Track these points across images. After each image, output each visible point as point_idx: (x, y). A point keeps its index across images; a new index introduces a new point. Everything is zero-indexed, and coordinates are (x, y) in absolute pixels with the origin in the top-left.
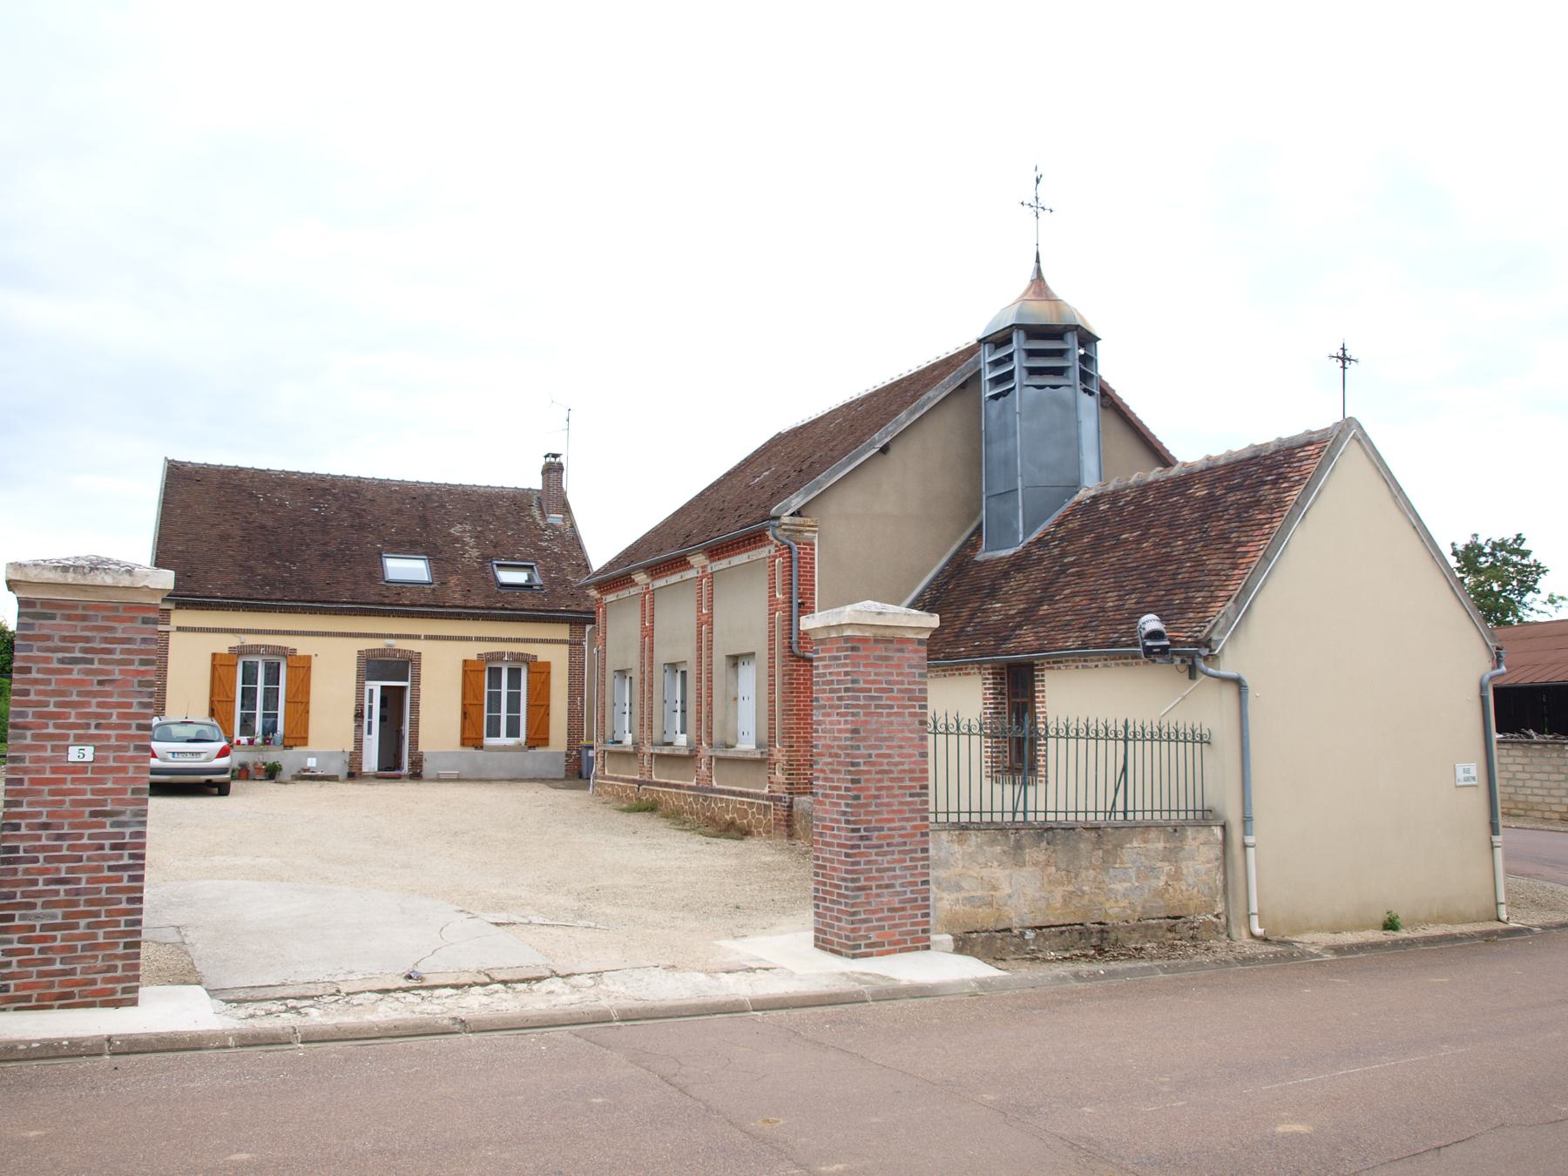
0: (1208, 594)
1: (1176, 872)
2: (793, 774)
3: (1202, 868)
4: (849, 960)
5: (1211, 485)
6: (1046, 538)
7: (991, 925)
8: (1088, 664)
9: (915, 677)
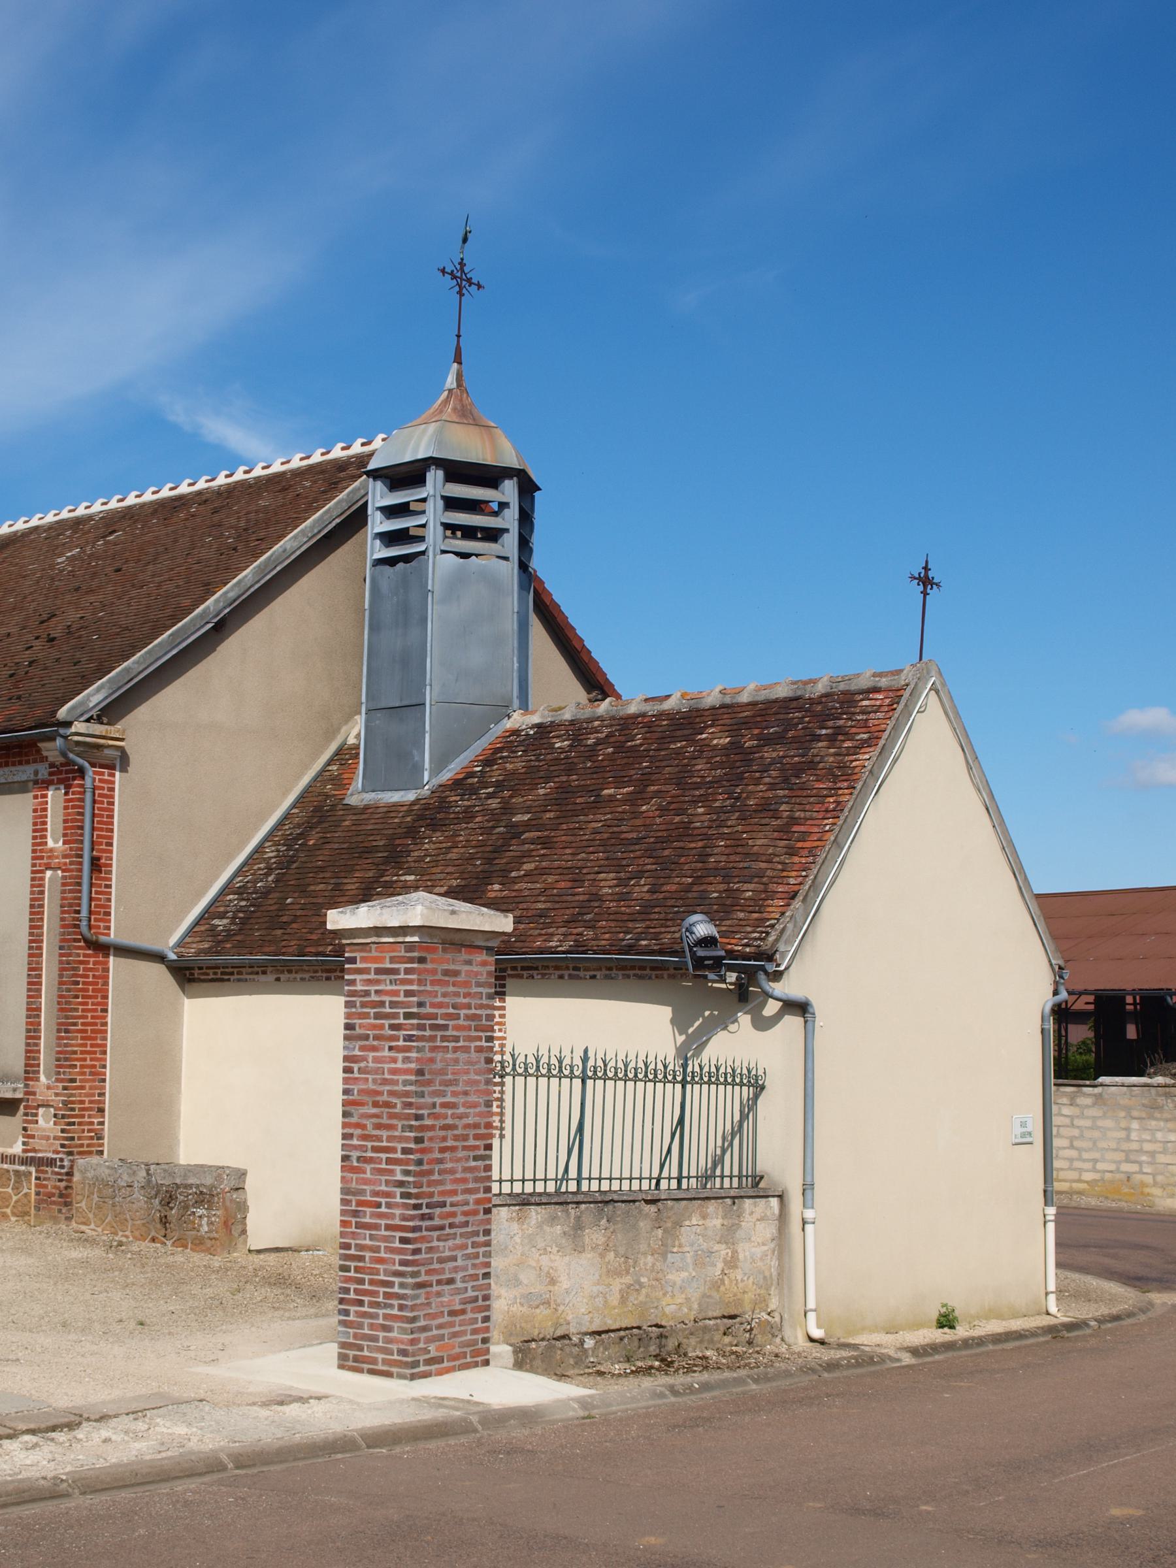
0: (762, 887)
1: (732, 1257)
2: (73, 1124)
3: (759, 1251)
4: (406, 1382)
5: (735, 729)
6: (470, 781)
7: (549, 1332)
8: (581, 973)
9: (482, 998)
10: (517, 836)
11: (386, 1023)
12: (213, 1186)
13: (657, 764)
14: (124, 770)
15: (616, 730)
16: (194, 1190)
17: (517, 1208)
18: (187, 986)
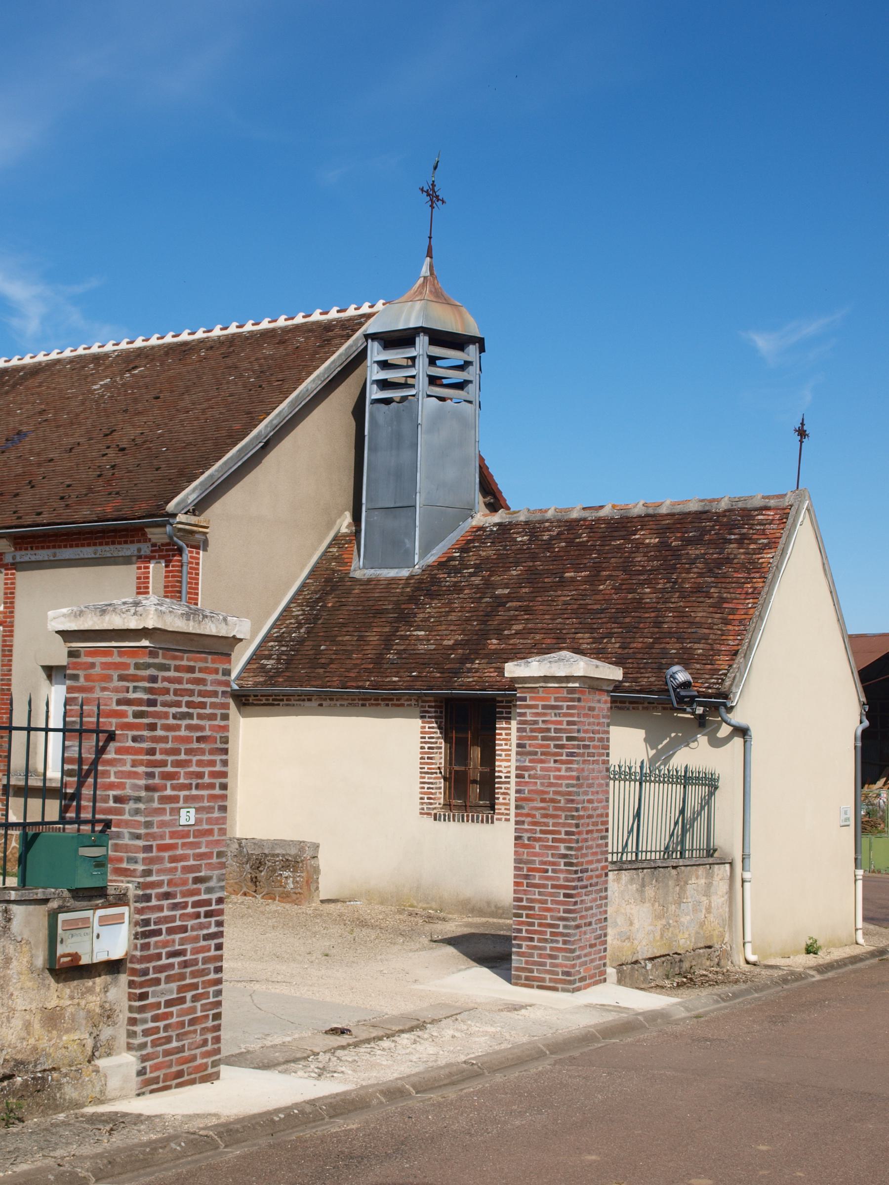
0: (708, 647)
6: (452, 563)
7: (631, 959)
10: (503, 604)
11: (552, 743)
12: (295, 856)
13: (604, 555)
14: (205, 550)
15: (564, 530)
16: (281, 858)
17: (617, 872)
18: (242, 708)
